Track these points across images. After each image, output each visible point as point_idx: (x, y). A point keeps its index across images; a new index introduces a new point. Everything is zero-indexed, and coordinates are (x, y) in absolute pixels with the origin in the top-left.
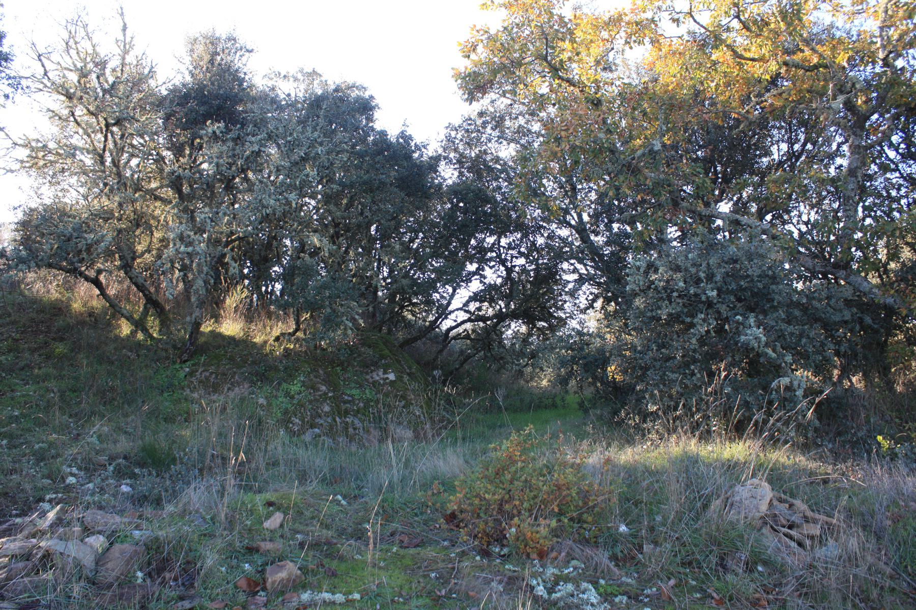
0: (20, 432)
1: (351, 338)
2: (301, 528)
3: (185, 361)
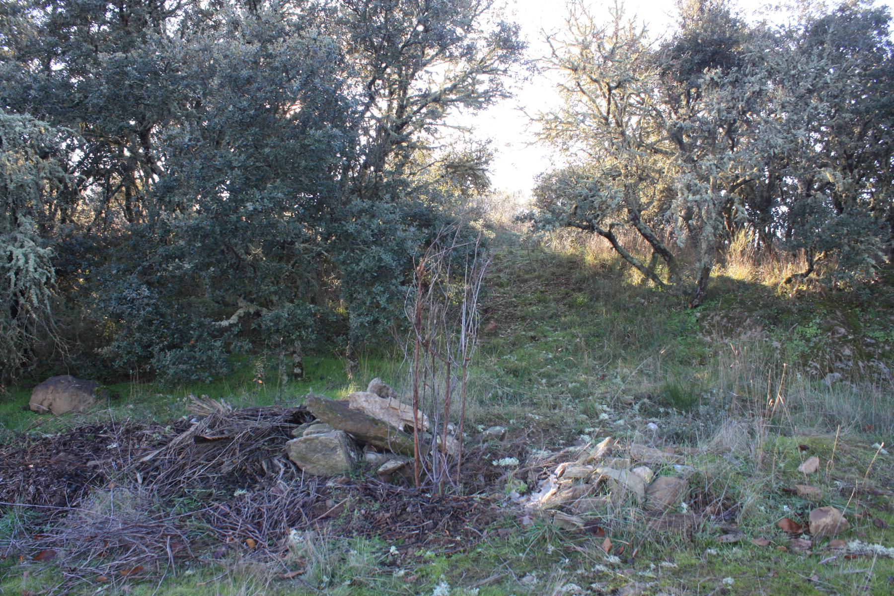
0: (555, 373)
1: (874, 277)
2: (839, 474)
3: (696, 306)
